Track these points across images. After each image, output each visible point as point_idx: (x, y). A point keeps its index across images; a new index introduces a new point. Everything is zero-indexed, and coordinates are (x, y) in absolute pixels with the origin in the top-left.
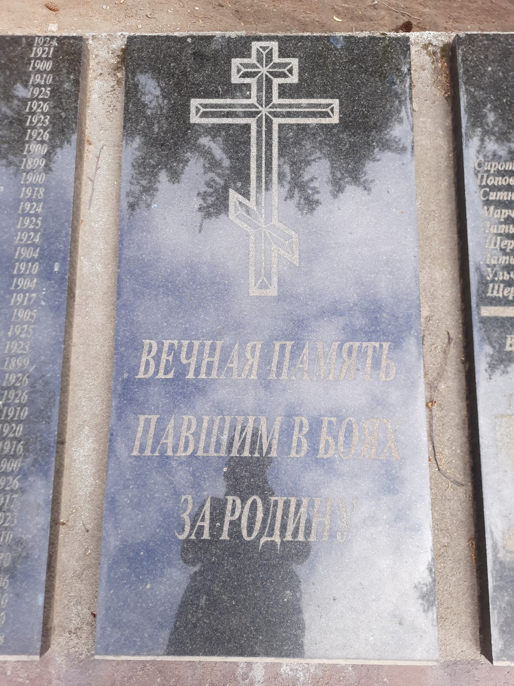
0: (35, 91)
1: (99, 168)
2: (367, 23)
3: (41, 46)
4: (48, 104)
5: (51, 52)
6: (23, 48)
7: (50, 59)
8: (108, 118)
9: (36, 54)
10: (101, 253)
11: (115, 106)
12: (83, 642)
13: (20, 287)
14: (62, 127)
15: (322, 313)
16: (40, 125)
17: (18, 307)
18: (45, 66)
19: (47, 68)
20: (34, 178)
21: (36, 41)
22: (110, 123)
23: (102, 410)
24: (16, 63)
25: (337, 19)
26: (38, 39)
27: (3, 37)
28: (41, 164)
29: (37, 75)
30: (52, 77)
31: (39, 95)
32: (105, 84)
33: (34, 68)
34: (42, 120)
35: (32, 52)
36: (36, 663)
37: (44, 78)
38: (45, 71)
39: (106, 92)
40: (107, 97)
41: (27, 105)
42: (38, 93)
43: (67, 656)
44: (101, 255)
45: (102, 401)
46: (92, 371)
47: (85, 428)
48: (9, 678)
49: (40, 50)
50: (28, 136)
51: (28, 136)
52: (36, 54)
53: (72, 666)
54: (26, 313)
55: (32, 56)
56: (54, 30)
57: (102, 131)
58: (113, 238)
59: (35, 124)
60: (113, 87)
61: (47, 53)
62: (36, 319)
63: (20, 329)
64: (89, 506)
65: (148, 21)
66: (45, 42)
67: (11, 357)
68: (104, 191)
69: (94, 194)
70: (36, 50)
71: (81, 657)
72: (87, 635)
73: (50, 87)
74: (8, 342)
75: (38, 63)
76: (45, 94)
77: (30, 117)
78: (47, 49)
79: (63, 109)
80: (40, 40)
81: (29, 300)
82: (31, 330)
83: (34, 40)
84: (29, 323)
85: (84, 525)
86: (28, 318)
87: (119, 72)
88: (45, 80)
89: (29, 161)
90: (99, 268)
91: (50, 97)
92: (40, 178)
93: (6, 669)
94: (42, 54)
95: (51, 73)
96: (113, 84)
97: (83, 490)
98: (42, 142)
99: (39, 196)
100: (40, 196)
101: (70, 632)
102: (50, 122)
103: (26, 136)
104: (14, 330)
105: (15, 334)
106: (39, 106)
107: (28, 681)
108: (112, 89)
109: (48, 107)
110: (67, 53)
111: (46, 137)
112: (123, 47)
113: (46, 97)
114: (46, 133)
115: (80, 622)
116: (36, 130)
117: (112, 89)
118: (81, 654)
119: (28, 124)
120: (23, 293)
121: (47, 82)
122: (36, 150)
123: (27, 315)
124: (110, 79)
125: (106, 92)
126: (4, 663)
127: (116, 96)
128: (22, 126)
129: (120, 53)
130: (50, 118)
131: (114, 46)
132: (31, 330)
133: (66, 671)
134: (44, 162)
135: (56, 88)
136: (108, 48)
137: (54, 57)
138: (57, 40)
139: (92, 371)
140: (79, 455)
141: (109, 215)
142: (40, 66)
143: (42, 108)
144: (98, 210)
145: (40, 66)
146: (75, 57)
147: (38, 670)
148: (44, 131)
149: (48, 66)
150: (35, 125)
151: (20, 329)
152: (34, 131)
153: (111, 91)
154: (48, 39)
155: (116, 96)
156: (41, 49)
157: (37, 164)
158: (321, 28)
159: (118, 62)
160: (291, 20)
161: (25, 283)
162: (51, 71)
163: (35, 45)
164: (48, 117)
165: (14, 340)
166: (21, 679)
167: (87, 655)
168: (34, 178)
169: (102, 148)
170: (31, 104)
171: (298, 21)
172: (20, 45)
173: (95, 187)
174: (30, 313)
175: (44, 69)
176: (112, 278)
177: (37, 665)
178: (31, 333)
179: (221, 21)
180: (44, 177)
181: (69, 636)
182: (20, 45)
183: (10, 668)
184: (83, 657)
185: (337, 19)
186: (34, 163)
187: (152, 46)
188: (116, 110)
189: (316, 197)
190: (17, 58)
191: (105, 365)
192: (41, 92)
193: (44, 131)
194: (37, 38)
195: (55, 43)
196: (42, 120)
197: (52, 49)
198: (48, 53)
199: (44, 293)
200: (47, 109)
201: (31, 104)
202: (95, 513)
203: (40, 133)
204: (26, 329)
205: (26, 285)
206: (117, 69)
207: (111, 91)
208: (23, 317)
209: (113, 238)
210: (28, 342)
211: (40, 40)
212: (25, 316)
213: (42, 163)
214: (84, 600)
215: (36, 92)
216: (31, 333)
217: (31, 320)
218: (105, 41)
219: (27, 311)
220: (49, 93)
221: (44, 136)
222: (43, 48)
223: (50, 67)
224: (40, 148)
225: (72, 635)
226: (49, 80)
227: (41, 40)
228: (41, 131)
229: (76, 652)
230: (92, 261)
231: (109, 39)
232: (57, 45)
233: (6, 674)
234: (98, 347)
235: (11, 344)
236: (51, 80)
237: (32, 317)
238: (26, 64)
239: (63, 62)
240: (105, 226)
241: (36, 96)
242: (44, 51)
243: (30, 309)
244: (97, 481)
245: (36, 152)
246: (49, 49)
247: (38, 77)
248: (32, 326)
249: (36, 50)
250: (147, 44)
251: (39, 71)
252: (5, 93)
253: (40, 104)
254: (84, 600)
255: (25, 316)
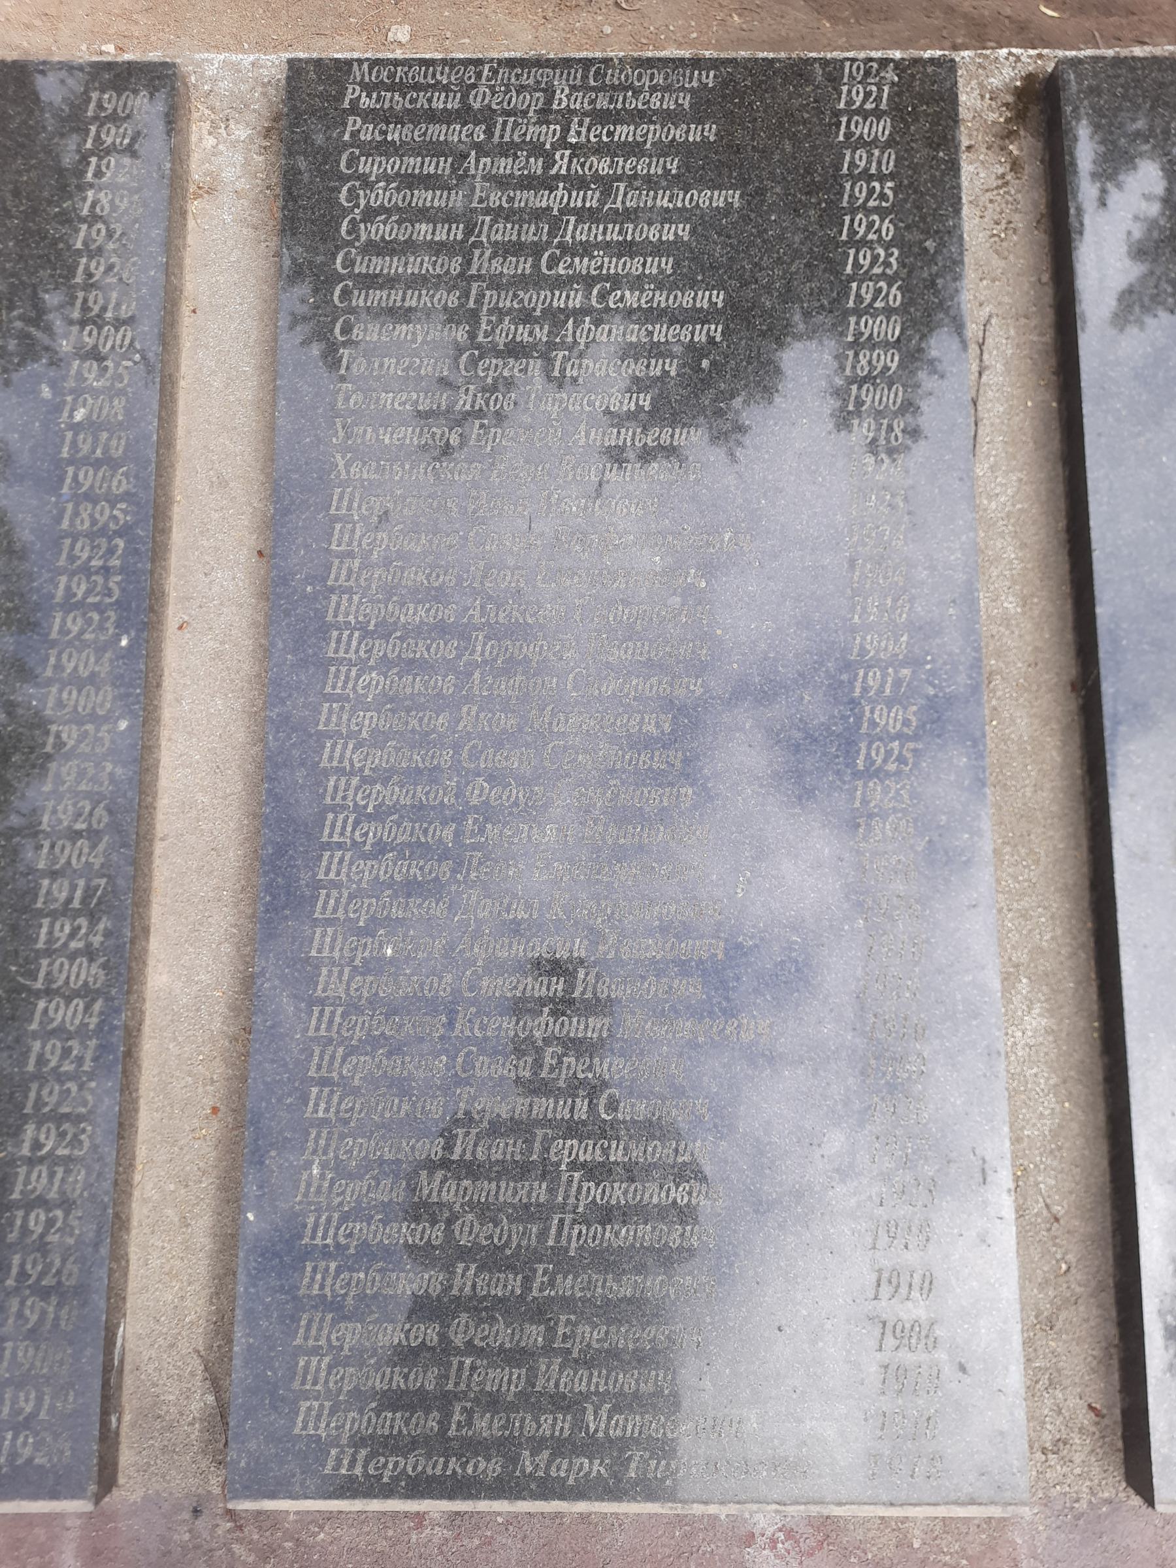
0: (857, 190)
1: (987, 368)
2: (1124, 21)
3: (859, 83)
4: (890, 222)
5: (885, 95)
6: (818, 87)
7: (885, 112)
8: (997, 252)
9: (850, 102)
10: (1011, 569)
11: (1010, 222)
12: (1078, 1471)
13: (871, 654)
14: (931, 275)
15: (740, 692)
16: (877, 270)
17: (873, 702)
18: (874, 129)
19: (880, 134)
20: (877, 398)
21: (847, 71)
22: (1002, 263)
23: (1052, 938)
24: (804, 122)
25: (1050, 13)
26: (851, 66)
27: (3, 62)
28: (889, 364)
29: (858, 152)
30: (893, 157)
31: (867, 200)
32: (980, 170)
33: (848, 135)
34: (881, 260)
35: (840, 98)
36: (976, 1522)
37: (875, 159)
38: (875, 142)
39: (987, 191)
40: (991, 201)
41: (842, 225)
42: (864, 194)
43: (1046, 1505)
44: (1012, 575)
45: (1052, 917)
46: (1020, 848)
47: (1020, 981)
48: (920, 1555)
49: (858, 92)
50: (852, 298)
51: (852, 298)
52: (850, 102)
53: (1059, 1527)
54: (892, 715)
55: (842, 106)
56: (404, 41)
57: (985, 282)
58: (1036, 534)
59: (865, 268)
60: (1003, 176)
61: (875, 100)
62: (917, 727)
63: (882, 750)
64: (1055, 1163)
65: (622, 18)
66: (867, 73)
67: (871, 816)
68: (1003, 423)
69: (980, 432)
70: (849, 92)
71: (1076, 1505)
72: (1083, 1457)
73: (893, 180)
74: (860, 783)
75: (857, 123)
76: (883, 196)
77: (852, 252)
78: (874, 88)
79: (928, 232)
80: (855, 67)
81: (898, 683)
82: (909, 755)
83: (842, 68)
84: (899, 736)
85: (1047, 1206)
86: (898, 726)
87: (1012, 143)
88: (879, 163)
89: (861, 357)
90: (1011, 605)
91: (893, 205)
92: (892, 396)
93: (909, 1536)
94: (864, 102)
95: (890, 147)
96: (1001, 171)
97: (1034, 1125)
98: (889, 312)
99: (893, 438)
100: (897, 440)
101: (1044, 1451)
102: (902, 264)
103: (848, 298)
104: (868, 754)
105: (873, 762)
106: (871, 225)
107: (964, 1562)
108: (1000, 182)
109: (892, 228)
110: (922, 98)
111: (896, 297)
112: (1018, 83)
113: (884, 204)
114: (894, 290)
115: (1063, 1428)
116: (871, 284)
117: (1000, 182)
118: (1077, 1501)
119: (849, 269)
120: (879, 668)
121: (884, 168)
122: (876, 330)
123: (895, 720)
124: (992, 157)
125: (987, 191)
126: (902, 1523)
127: (1010, 199)
128: (838, 273)
129: (1010, 99)
130: (900, 255)
131: (995, 82)
132: (909, 755)
133: (1050, 1539)
134: (896, 358)
135: (906, 182)
136: (981, 85)
137: (893, 109)
138: (896, 68)
139: (1020, 848)
140: (1015, 1044)
141: (1020, 480)
142: (863, 129)
143: (879, 231)
144: (992, 468)
145: (863, 129)
146: (943, 109)
147: (984, 1536)
148: (890, 286)
149: (881, 129)
150: (866, 272)
151: (882, 750)
152: (865, 285)
153: (998, 188)
154: (875, 65)
155: (1010, 199)
156: (861, 90)
157: (882, 363)
158: (1019, 33)
159: (1008, 120)
160: (946, 13)
161: (883, 644)
162: (891, 142)
163: (845, 80)
164: (896, 252)
165: (871, 777)
166: (948, 1558)
167: (1090, 1502)
168: (877, 398)
169: (988, 321)
170: (852, 221)
171: (965, 16)
172: (808, 81)
173: (980, 414)
174: (900, 713)
175: (872, 137)
176: (1042, 629)
177: (978, 1526)
178: (911, 761)
179: (782, 17)
180: (900, 394)
181: (1044, 1458)
182: (808, 81)
183: (917, 1532)
184: (1082, 1506)
185: (1050, 13)
186: (874, 362)
187: (1122, 80)
188: (1015, 231)
189: (863, 429)
190: (808, 112)
191: (1051, 833)
192: (871, 191)
193: (890, 286)
194: (848, 64)
195: (891, 75)
196: (881, 260)
197: (886, 89)
198: (878, 99)
199: (928, 667)
200: (891, 234)
201: (852, 221)
202: (1070, 1178)
203: (880, 290)
204: (896, 752)
205: (886, 649)
206: (1010, 135)
207: (998, 188)
208: (887, 723)
209: (1036, 534)
210: (906, 781)
211: (855, 67)
212: (891, 721)
213: (892, 361)
214: (1068, 1377)
215: (860, 192)
216: (911, 761)
217: (905, 730)
218: (973, 68)
219: (894, 710)
220: (890, 193)
221: (891, 298)
222: (865, 88)
223: (887, 132)
224: (884, 326)
225: (1051, 1456)
226: (888, 163)
227: (858, 68)
228: (882, 284)
229: (1065, 1494)
230: (992, 588)
231: (980, 66)
232: (896, 79)
233: (911, 1546)
234: (1029, 791)
235: (865, 786)
236: (892, 164)
237: (906, 723)
238: (830, 125)
239: (916, 120)
240: (1014, 505)
241: (861, 201)
242: (868, 95)
243: (900, 703)
244: (1067, 1105)
245: (875, 335)
246: (880, 90)
247: (861, 157)
248: (911, 745)
249: (849, 92)
250: (1109, 76)
251: (861, 143)
252: (787, 195)
253: (874, 221)
254: (1068, 1377)
255: (891, 721)
